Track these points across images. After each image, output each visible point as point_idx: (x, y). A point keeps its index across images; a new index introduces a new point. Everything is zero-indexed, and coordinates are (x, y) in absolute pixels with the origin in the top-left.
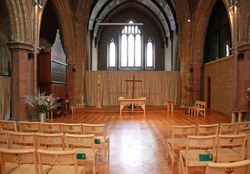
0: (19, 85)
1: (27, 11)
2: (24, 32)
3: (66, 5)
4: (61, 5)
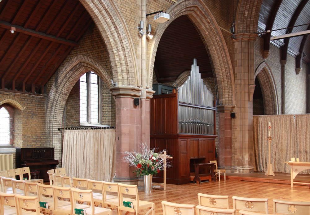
0: (121, 139)
1: (129, 47)
2: (127, 73)
3: (211, 20)
4: (203, 22)
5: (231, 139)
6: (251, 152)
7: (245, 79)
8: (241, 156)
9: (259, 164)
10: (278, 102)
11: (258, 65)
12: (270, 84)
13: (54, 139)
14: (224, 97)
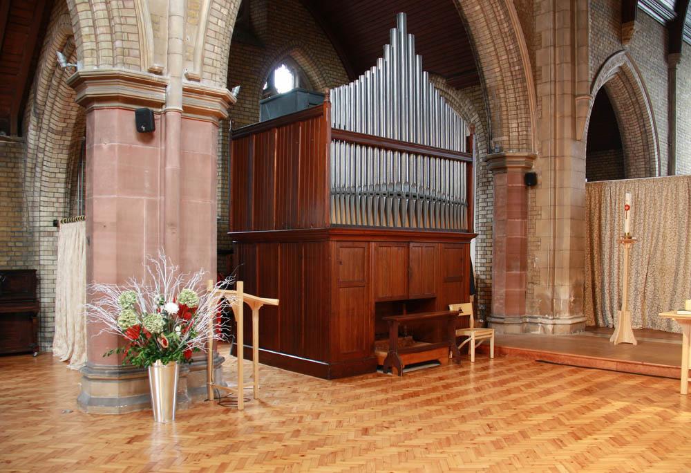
5: (524, 244)
6: (579, 278)
7: (563, 81)
8: (551, 289)
9: (602, 307)
10: (659, 154)
11: (606, 58)
12: (640, 108)
13: (42, 248)
14: (505, 130)
